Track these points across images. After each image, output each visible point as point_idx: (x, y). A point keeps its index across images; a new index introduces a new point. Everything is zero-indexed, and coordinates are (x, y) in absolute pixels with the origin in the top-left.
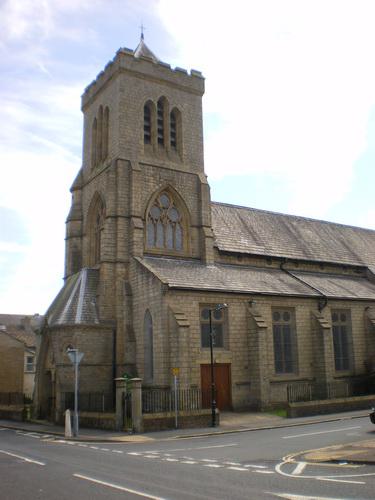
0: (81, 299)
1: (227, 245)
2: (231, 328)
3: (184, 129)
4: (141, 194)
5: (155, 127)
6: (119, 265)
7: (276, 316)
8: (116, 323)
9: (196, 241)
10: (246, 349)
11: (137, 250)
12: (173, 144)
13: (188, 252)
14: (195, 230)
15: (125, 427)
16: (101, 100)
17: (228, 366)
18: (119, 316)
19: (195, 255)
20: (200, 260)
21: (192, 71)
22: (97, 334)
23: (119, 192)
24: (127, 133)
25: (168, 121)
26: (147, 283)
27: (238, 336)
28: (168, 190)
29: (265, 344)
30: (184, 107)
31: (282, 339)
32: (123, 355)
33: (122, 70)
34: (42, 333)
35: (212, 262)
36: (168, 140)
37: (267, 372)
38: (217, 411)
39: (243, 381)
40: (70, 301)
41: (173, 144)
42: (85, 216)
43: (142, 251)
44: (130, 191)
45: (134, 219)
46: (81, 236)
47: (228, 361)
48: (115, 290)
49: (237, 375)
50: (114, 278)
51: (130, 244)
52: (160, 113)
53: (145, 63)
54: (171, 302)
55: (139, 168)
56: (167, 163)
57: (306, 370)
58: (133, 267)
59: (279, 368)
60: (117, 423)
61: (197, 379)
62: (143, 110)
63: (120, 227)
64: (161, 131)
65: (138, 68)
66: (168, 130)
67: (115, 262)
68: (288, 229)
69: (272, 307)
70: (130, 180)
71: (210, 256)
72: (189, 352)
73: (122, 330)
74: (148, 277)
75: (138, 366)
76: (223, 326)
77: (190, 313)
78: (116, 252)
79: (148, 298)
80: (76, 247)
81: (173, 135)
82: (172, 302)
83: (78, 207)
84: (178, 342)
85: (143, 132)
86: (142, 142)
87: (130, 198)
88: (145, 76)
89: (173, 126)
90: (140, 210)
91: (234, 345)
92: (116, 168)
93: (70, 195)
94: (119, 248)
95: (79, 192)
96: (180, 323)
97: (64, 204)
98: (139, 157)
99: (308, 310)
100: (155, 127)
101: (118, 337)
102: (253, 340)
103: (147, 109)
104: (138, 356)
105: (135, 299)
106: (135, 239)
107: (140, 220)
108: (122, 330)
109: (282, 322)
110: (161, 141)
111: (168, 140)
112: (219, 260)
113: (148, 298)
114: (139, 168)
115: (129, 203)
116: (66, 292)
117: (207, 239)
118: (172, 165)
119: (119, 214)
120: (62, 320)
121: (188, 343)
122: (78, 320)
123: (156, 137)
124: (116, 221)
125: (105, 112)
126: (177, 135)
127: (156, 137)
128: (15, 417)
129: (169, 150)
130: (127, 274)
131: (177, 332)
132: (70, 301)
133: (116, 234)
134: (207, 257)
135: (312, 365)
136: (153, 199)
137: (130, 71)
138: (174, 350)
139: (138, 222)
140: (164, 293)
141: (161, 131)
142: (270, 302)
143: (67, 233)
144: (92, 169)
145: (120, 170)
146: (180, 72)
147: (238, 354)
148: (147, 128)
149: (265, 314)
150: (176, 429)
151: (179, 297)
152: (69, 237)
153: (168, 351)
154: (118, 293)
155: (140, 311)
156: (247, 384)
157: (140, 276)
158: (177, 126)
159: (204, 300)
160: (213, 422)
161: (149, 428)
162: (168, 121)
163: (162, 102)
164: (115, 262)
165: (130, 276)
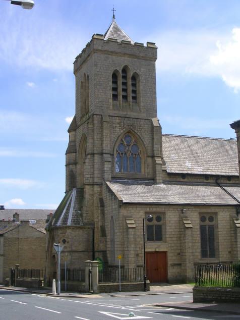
0: (72, 209)
1: (172, 168)
2: (167, 228)
3: (141, 87)
4: (109, 139)
5: (120, 87)
6: (95, 186)
7: (203, 219)
8: (94, 225)
9: (151, 167)
10: (179, 242)
11: (107, 176)
12: (134, 98)
13: (145, 175)
14: (150, 160)
15: (89, 291)
16: (84, 69)
17: (165, 253)
18: (96, 220)
19: (149, 177)
20: (151, 181)
21: (148, 43)
22: (81, 231)
23: (95, 137)
24: (103, 94)
25: (130, 82)
26: (112, 199)
27: (173, 233)
28: (129, 133)
29: (191, 238)
30: (141, 71)
31: (208, 235)
32: (99, 245)
33: (96, 51)
34: (49, 231)
35: (161, 181)
36: (130, 95)
37: (191, 257)
38: (148, 281)
39: (177, 263)
40: (66, 207)
41: (134, 98)
42: (77, 149)
43: (110, 176)
44: (102, 136)
45: (104, 155)
46: (75, 164)
47: (165, 250)
48: (93, 203)
49: (171, 259)
50: (93, 195)
51: (102, 171)
52: (125, 77)
53: (112, 43)
54: (124, 212)
55: (108, 119)
56: (129, 113)
57: (225, 256)
58: (104, 187)
59: (204, 254)
60: (86, 287)
61: (141, 262)
62: (111, 78)
63: (96, 161)
64: (125, 90)
65: (106, 48)
66: (130, 89)
67: (93, 185)
68: (227, 151)
69: (200, 213)
70: (102, 128)
71: (159, 177)
72: (135, 244)
73: (98, 228)
74: (112, 195)
75: (108, 252)
76: (163, 227)
77: (136, 221)
78: (93, 178)
79: (112, 209)
80: (72, 171)
81: (134, 92)
82: (125, 212)
83: (72, 144)
84: (128, 238)
85: (111, 93)
86: (111, 101)
87: (102, 141)
88: (112, 53)
89: (134, 85)
90: (109, 149)
91: (170, 239)
92: (93, 120)
93: (68, 134)
94: (96, 175)
95: (74, 133)
96: (129, 226)
97: (65, 139)
98: (109, 111)
99: (228, 214)
100: (120, 87)
101: (95, 234)
102: (183, 236)
103: (115, 76)
104: (108, 246)
105: (105, 209)
106: (105, 169)
107: (109, 156)
108: (98, 228)
109: (207, 223)
110: (125, 97)
111: (130, 95)
112: (168, 179)
113: (112, 209)
114: (108, 119)
115: (102, 144)
116: (63, 205)
117: (157, 165)
118: (133, 114)
119: (95, 152)
120: (59, 223)
121: (135, 238)
122: (69, 223)
123: (121, 93)
124: (94, 156)
125: (87, 78)
126: (137, 92)
127: (121, 93)
128: (34, 286)
129: (131, 103)
130: (101, 192)
131: (127, 231)
132: (66, 207)
133: (94, 165)
134: (157, 178)
135: (230, 252)
136: (120, 139)
137: (101, 51)
138: (126, 243)
139: (107, 157)
140: (120, 207)
141: (125, 90)
142: (198, 210)
143: (66, 162)
144: (81, 118)
145: (95, 122)
146: (139, 46)
147: (173, 245)
148: (115, 89)
149: (193, 221)
150: (120, 292)
151: (131, 209)
152: (68, 165)
153: (123, 243)
154: (95, 205)
155: (108, 217)
156: (180, 265)
157: (108, 194)
158: (137, 85)
159: (148, 210)
160: (145, 288)
161: (102, 290)
162: (130, 82)
163: (125, 70)
164: (93, 185)
165: (103, 193)
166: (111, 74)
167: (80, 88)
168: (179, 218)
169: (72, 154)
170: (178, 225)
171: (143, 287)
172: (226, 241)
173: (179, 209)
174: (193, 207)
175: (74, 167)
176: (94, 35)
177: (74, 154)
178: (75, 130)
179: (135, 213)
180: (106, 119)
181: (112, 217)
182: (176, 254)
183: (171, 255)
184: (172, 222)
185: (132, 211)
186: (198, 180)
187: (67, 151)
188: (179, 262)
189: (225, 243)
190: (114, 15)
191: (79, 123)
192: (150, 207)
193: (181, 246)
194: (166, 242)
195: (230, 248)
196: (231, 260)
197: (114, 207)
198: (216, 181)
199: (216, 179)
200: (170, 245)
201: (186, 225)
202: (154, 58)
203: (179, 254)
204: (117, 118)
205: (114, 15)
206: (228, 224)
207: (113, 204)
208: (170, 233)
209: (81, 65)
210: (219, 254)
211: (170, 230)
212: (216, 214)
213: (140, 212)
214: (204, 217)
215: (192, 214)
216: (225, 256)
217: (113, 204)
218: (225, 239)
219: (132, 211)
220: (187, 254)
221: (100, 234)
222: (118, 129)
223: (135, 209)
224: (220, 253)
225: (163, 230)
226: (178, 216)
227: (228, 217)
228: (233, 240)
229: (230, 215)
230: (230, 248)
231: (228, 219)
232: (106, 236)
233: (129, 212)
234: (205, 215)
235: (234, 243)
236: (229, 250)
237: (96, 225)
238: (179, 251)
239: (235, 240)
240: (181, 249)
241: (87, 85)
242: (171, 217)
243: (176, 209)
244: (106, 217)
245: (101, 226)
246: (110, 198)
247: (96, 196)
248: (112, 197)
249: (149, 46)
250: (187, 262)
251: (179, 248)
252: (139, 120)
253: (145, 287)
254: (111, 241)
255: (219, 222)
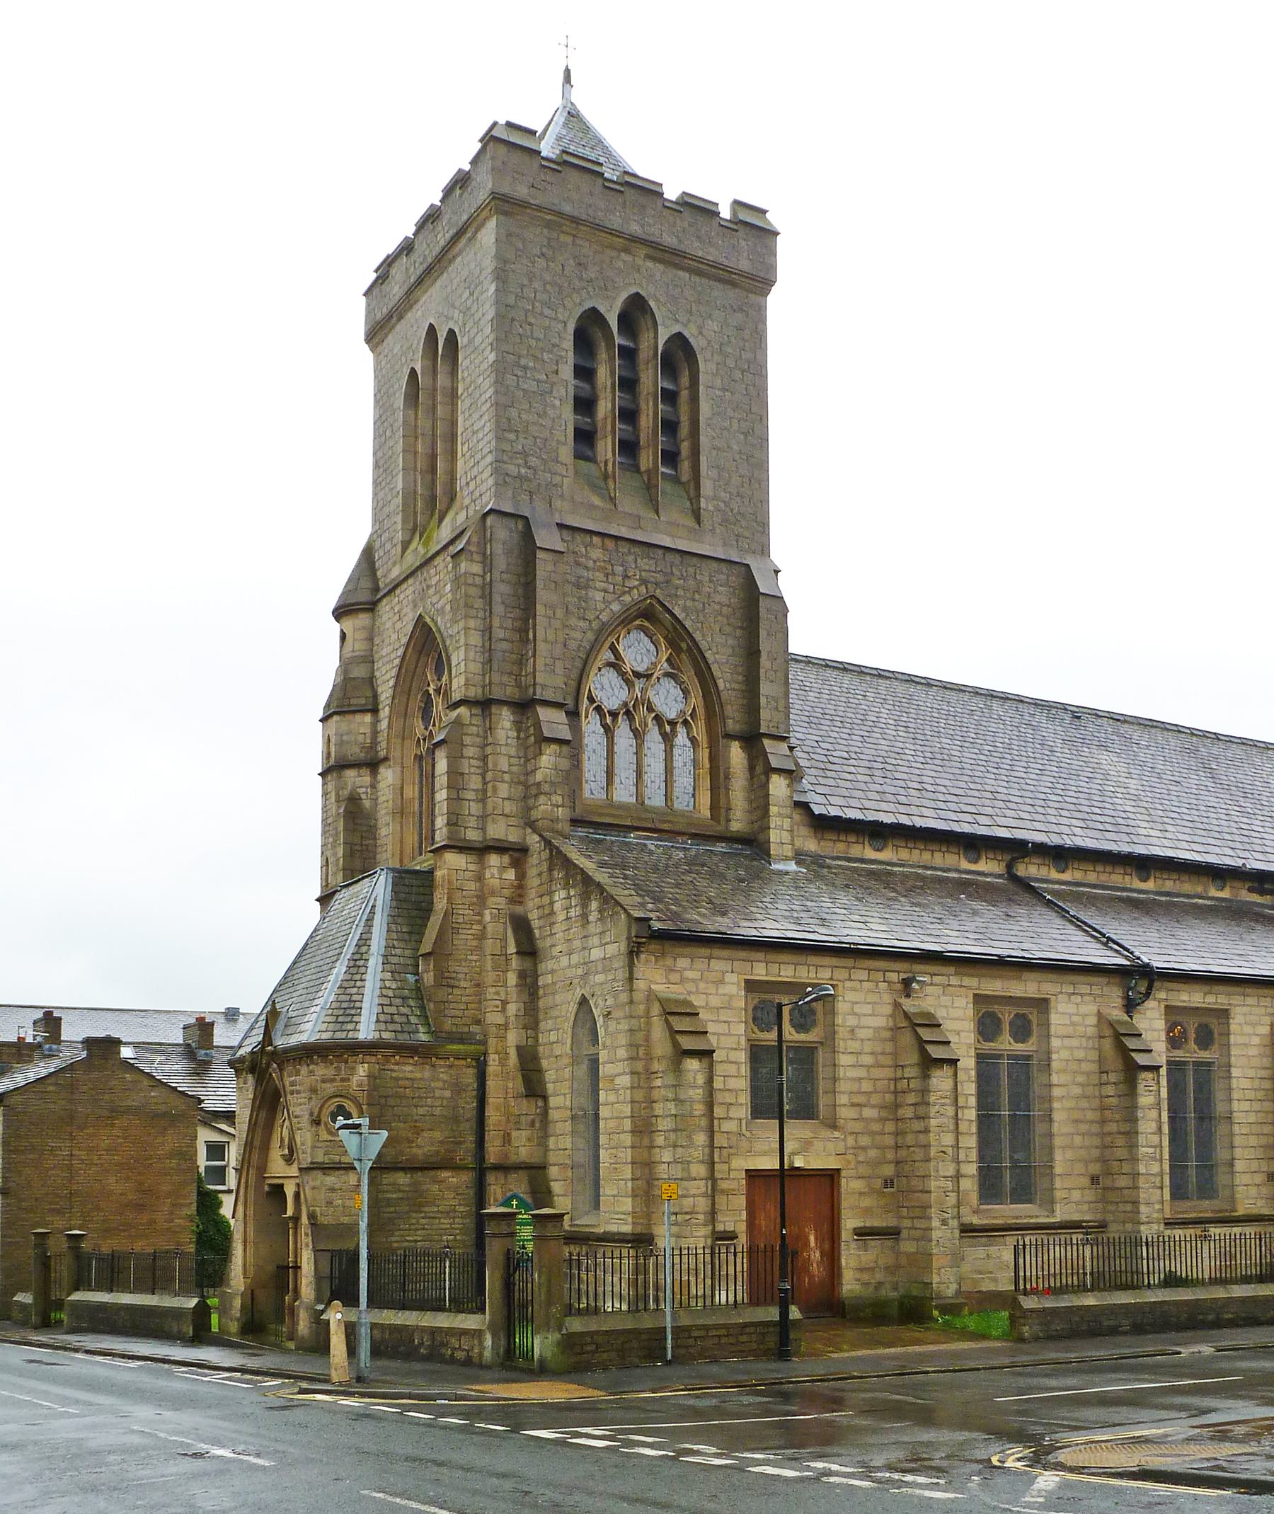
2: (844, 1060)
6: (494, 860)
10: (890, 1127)
12: (671, 457)
17: (832, 1176)
18: (494, 1018)
25: (650, 379)
26: (584, 916)
39: (877, 1223)
41: (671, 457)
47: (832, 1164)
48: (482, 937)
53: (573, 176)
57: (1076, 1195)
59: (990, 1188)
62: (568, 343)
69: (979, 999)
75: (553, 1171)
76: (822, 1056)
81: (670, 427)
85: (568, 417)
95: (363, 619)
101: (490, 1084)
102: (911, 1098)
105: (542, 967)
135: (1094, 1180)
147: (865, 1140)
148: (585, 405)
151: (683, 963)
156: (892, 1233)
159: (760, 972)
166: (571, 327)
167: (400, 402)
168: (893, 1016)
169: (358, 717)
170: (889, 1047)
171: (772, 1342)
172: (1083, 1127)
173: (893, 977)
174: (951, 970)
175: (368, 780)
176: (495, 124)
177: (368, 718)
178: (371, 607)
179: (702, 985)
180: (546, 538)
181: (584, 1002)
182: (878, 1183)
183: (857, 1185)
184: (862, 1033)
185: (689, 974)
186: (938, 855)
187: (327, 706)
188: (889, 1221)
189: (1078, 1140)
190: (567, 73)
191: (396, 572)
192: (771, 957)
193: (897, 1147)
194: (834, 1126)
195: (1097, 1160)
196: (1099, 1217)
197: (596, 954)
198: (1010, 867)
199: (1008, 857)
200: (850, 1141)
201: (930, 1048)
202: (762, 282)
203: (888, 1183)
204: (596, 539)
205: (567, 73)
206: (1094, 1055)
207: (595, 940)
208: (855, 1087)
209: (410, 292)
210: (1053, 1189)
211: (852, 1073)
212: (1042, 1004)
213: (722, 982)
214: (992, 1015)
215: (945, 1000)
216: (1076, 1195)
217: (595, 940)
218: (1077, 1121)
219: (689, 974)
220: (933, 1184)
221: (516, 1084)
222: (599, 596)
223: (700, 964)
224: (1058, 1183)
225: (822, 1072)
226: (888, 1010)
227: (1093, 1020)
228: (1113, 1127)
229: (1099, 1014)
230: (1097, 1160)
231: (1091, 1031)
232: (545, 1098)
233: (675, 977)
234: (996, 1008)
235: (1120, 1141)
236: (1095, 1168)
237: (492, 1041)
238: (889, 1170)
239: (1125, 1127)
240: (897, 1163)
241: (443, 380)
242: (857, 1009)
243: (880, 976)
244: (541, 1003)
245: (519, 1048)
246: (578, 910)
247: (498, 902)
248: (585, 904)
249: (745, 216)
250: (935, 1223)
251: (890, 1155)
252: (695, 560)
253: (784, 1339)
254: (573, 1118)
255: (1055, 1043)
